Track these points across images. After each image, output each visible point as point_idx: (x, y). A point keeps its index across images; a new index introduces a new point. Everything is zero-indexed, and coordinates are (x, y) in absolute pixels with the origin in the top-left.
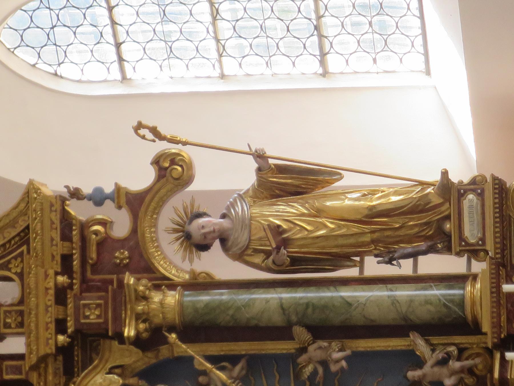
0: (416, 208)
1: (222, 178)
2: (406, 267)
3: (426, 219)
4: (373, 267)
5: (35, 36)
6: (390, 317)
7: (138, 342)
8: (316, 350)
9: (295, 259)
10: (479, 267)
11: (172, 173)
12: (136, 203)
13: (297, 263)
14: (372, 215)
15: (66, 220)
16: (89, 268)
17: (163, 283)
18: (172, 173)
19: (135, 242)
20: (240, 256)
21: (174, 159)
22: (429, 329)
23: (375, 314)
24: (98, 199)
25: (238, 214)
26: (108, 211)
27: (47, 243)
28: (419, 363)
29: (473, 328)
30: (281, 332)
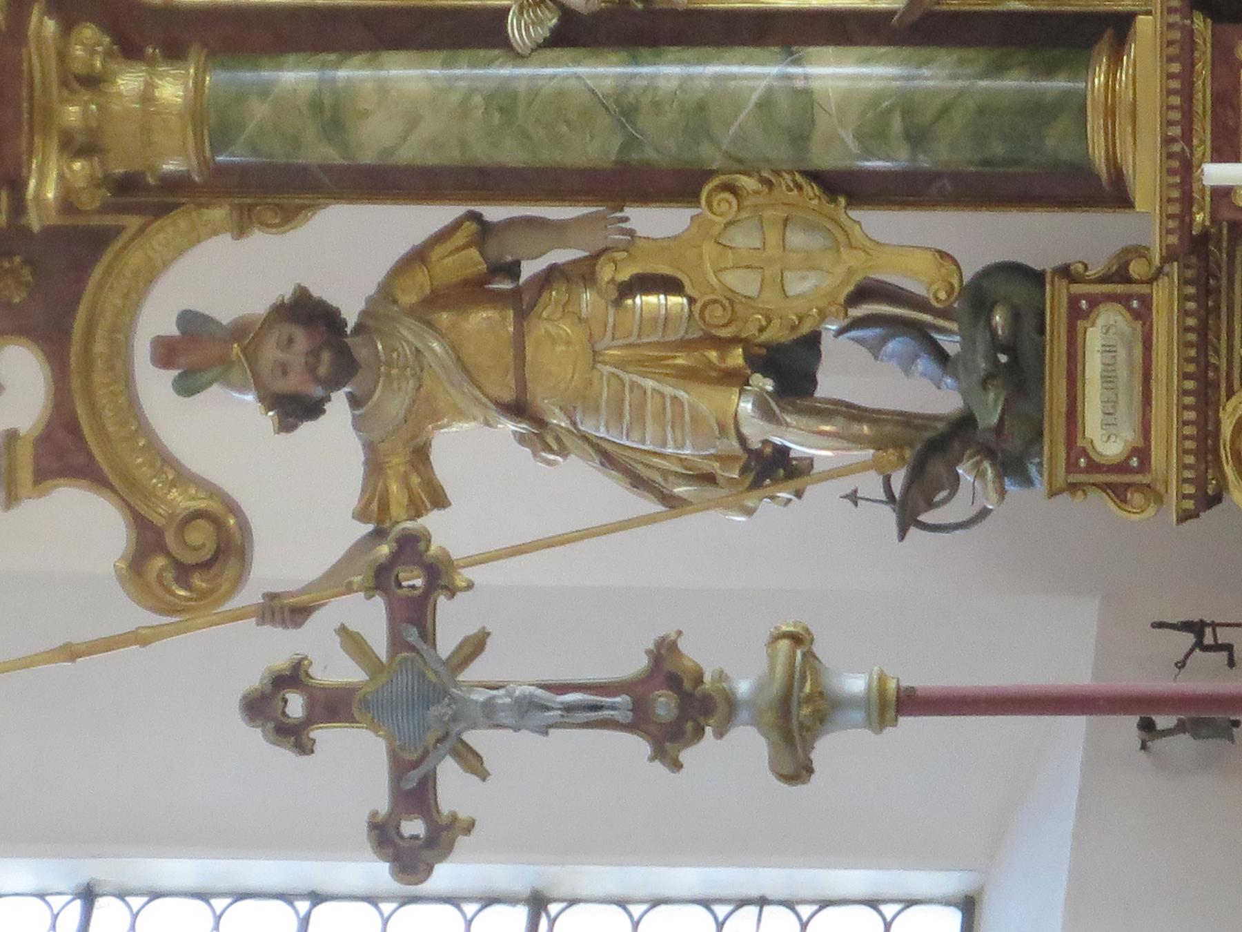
25: (913, 118)
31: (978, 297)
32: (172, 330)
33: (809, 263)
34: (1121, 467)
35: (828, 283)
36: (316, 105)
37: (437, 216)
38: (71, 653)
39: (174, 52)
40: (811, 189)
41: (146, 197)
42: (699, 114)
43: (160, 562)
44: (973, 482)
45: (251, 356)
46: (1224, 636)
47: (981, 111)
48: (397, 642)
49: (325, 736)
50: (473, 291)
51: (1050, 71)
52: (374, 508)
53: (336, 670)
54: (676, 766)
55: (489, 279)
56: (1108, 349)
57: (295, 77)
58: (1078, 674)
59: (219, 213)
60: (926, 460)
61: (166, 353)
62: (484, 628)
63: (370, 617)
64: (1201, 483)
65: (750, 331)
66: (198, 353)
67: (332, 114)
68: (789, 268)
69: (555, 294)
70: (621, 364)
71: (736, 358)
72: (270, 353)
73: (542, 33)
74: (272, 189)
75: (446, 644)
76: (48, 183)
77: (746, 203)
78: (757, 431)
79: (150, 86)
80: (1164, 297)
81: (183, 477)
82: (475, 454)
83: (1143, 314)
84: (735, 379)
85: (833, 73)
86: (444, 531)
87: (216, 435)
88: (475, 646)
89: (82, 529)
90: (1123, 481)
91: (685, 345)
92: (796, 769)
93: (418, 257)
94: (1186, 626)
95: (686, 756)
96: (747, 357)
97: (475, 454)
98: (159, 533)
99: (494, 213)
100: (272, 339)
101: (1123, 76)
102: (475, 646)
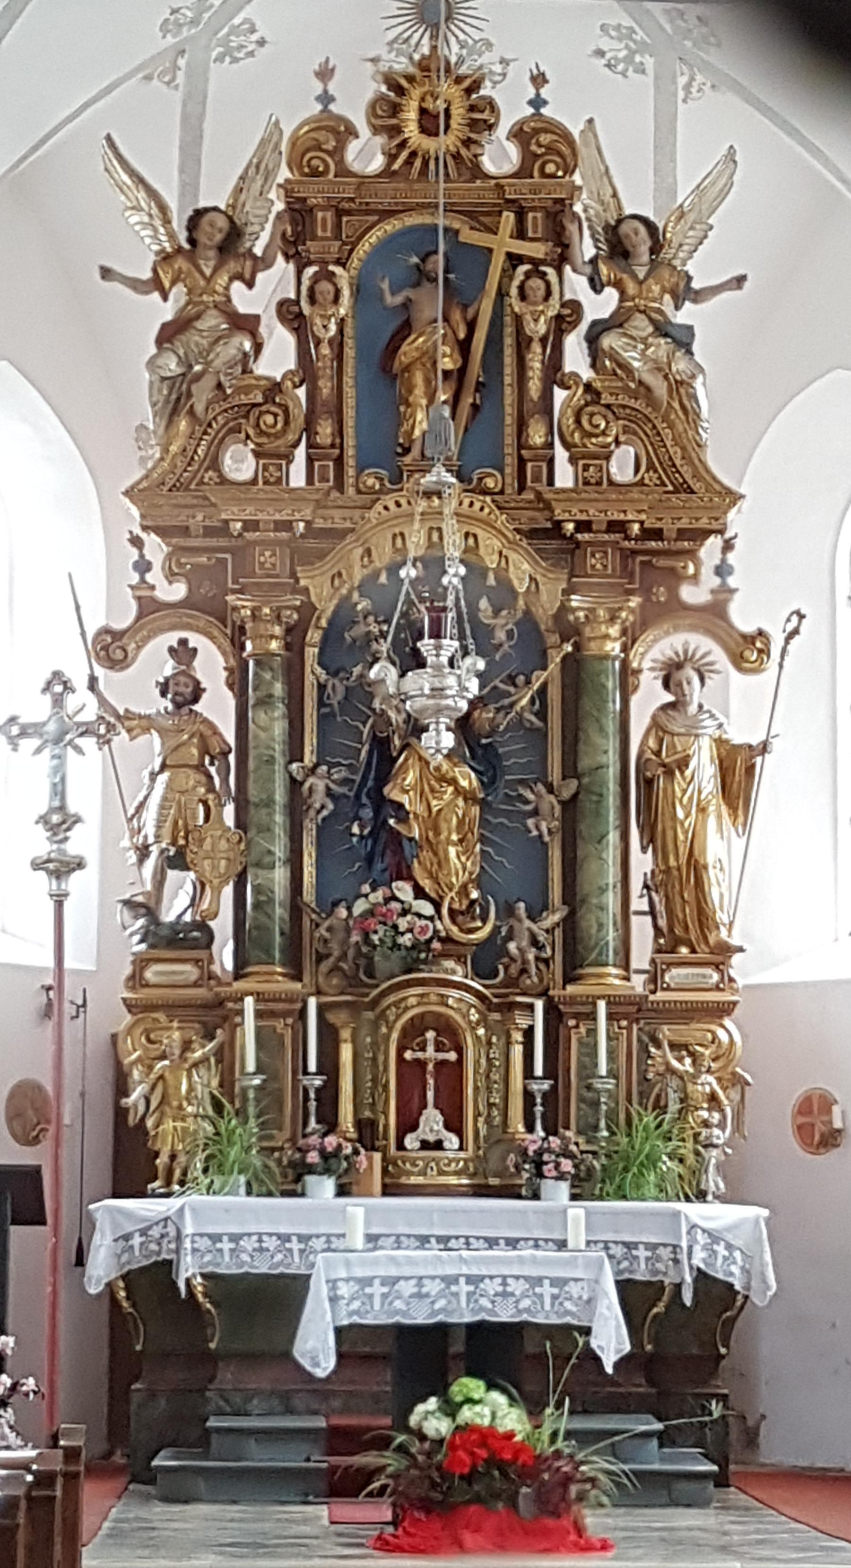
0: (704, 918)
2: (638, 903)
3: (689, 923)
7: (564, 609)
9: (652, 785)
10: (638, 983)
12: (714, 615)
13: (647, 784)
15: (706, 533)
18: (748, 650)
19: (673, 611)
20: (656, 726)
24: (722, 570)
29: (569, 979)
31: (202, 926)
32: (191, 645)
33: (214, 867)
34: (141, 977)
35: (207, 874)
36: (271, 696)
37: (231, 739)
38: (78, 608)
39: (288, 647)
40: (240, 868)
42: (267, 829)
43: (109, 640)
45: (183, 673)
46: (82, 1015)
47: (268, 929)
48: (79, 725)
49: (48, 698)
50: (205, 750)
51: (282, 951)
52: (129, 715)
53: (72, 702)
54: (37, 822)
56: (182, 973)
58: (69, 963)
59: (232, 662)
60: (146, 908)
61: (183, 642)
63: (90, 714)
64: (136, 1006)
65: (191, 847)
66: (183, 653)
69: (203, 779)
70: (179, 802)
71: (181, 842)
72: (182, 679)
73: (294, 774)
74: (237, 681)
75: (79, 741)
77: (460, 802)
78: (155, 850)
79: (277, 638)
80: (201, 992)
81: (139, 648)
83: (195, 985)
84: (174, 843)
85: (280, 876)
86: (121, 738)
87: (155, 659)
88: (79, 750)
90: (136, 980)
91: (186, 825)
92: (37, 865)
93: (216, 732)
94: (85, 1001)
95: (40, 826)
96: (182, 847)
98: (120, 639)
99: (232, 758)
100: (188, 680)
101: (280, 978)
102: (79, 750)
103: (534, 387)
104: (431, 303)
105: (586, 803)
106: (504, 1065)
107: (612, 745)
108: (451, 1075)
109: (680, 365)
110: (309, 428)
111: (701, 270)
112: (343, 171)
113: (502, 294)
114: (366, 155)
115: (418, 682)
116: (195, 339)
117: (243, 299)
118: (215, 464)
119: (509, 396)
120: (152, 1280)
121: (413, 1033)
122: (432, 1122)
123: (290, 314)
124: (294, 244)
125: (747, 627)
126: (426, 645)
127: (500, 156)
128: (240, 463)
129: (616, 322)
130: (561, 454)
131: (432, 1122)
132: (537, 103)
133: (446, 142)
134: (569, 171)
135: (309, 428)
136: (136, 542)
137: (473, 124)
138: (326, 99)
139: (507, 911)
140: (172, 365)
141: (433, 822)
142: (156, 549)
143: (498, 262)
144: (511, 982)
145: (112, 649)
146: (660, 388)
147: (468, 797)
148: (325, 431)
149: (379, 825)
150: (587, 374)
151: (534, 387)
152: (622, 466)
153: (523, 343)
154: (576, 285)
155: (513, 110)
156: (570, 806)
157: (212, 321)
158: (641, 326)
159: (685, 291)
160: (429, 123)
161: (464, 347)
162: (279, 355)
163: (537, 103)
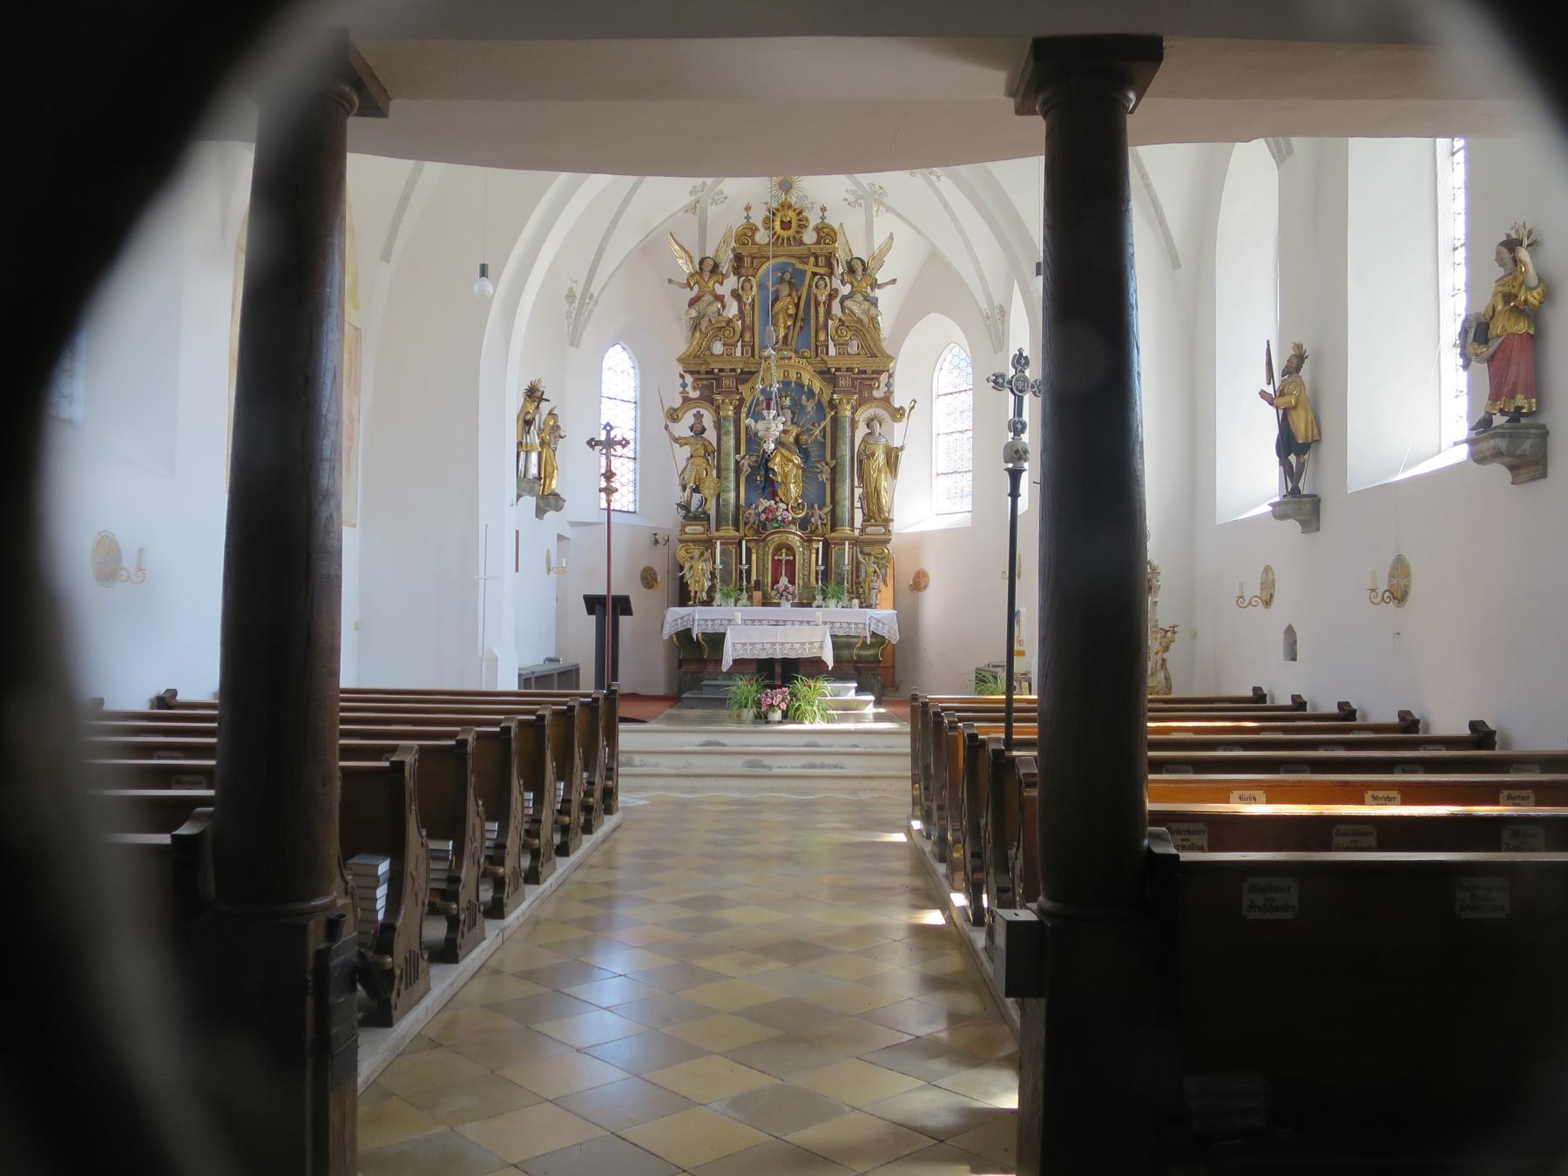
0: (880, 509)
1: (898, 434)
2: (857, 504)
3: (876, 513)
4: (858, 491)
5: (956, 360)
6: (838, 497)
7: (832, 400)
8: (827, 470)
9: (862, 461)
10: (857, 532)
11: (898, 414)
12: (886, 400)
13: (860, 462)
14: (878, 492)
15: (881, 372)
16: (744, 410)
17: (854, 410)
18: (898, 414)
19: (871, 399)
20: (864, 440)
21: (902, 415)
22: (833, 512)
23: (839, 493)
24: (888, 385)
25: (726, 505)
26: (883, 388)
27: (871, 365)
28: (820, 508)
29: (833, 530)
30: (834, 456)
41: (717, 410)
44: (683, 512)
53: (618, 447)
55: (707, 453)
57: (732, 428)
60: (685, 507)
62: (1019, 112)
66: (699, 416)
67: (727, 433)
68: (709, 490)
74: (718, 426)
76: (719, 398)
82: (687, 451)
85: (732, 495)
87: (688, 419)
89: (678, 403)
90: (683, 531)
97: (687, 451)
103: (821, 319)
104: (785, 289)
105: (839, 469)
106: (809, 560)
107: (848, 447)
108: (791, 565)
109: (873, 311)
110: (742, 336)
111: (881, 277)
112: (754, 243)
113: (810, 286)
114: (762, 237)
115: (760, 426)
116: (701, 305)
117: (719, 290)
118: (709, 348)
119: (813, 322)
120: (684, 636)
121: (778, 549)
122: (784, 581)
123: (736, 294)
124: (737, 270)
125: (897, 405)
126: (765, 412)
127: (809, 237)
128: (718, 348)
129: (850, 296)
130: (831, 344)
131: (784, 581)
132: (823, 218)
133: (791, 232)
134: (834, 241)
135: (742, 336)
136: (682, 377)
137: (800, 226)
138: (748, 218)
139: (811, 507)
140: (694, 313)
141: (786, 476)
142: (689, 379)
143: (808, 275)
144: (812, 532)
145: (673, 415)
146: (866, 320)
147: (798, 467)
148: (747, 336)
149: (766, 477)
150: (840, 315)
151: (821, 319)
152: (853, 348)
153: (817, 304)
154: (836, 283)
155: (814, 219)
156: (834, 470)
157: (708, 297)
158: (859, 297)
159: (875, 285)
160: (786, 225)
161: (797, 306)
162: (732, 309)
163: (823, 218)
